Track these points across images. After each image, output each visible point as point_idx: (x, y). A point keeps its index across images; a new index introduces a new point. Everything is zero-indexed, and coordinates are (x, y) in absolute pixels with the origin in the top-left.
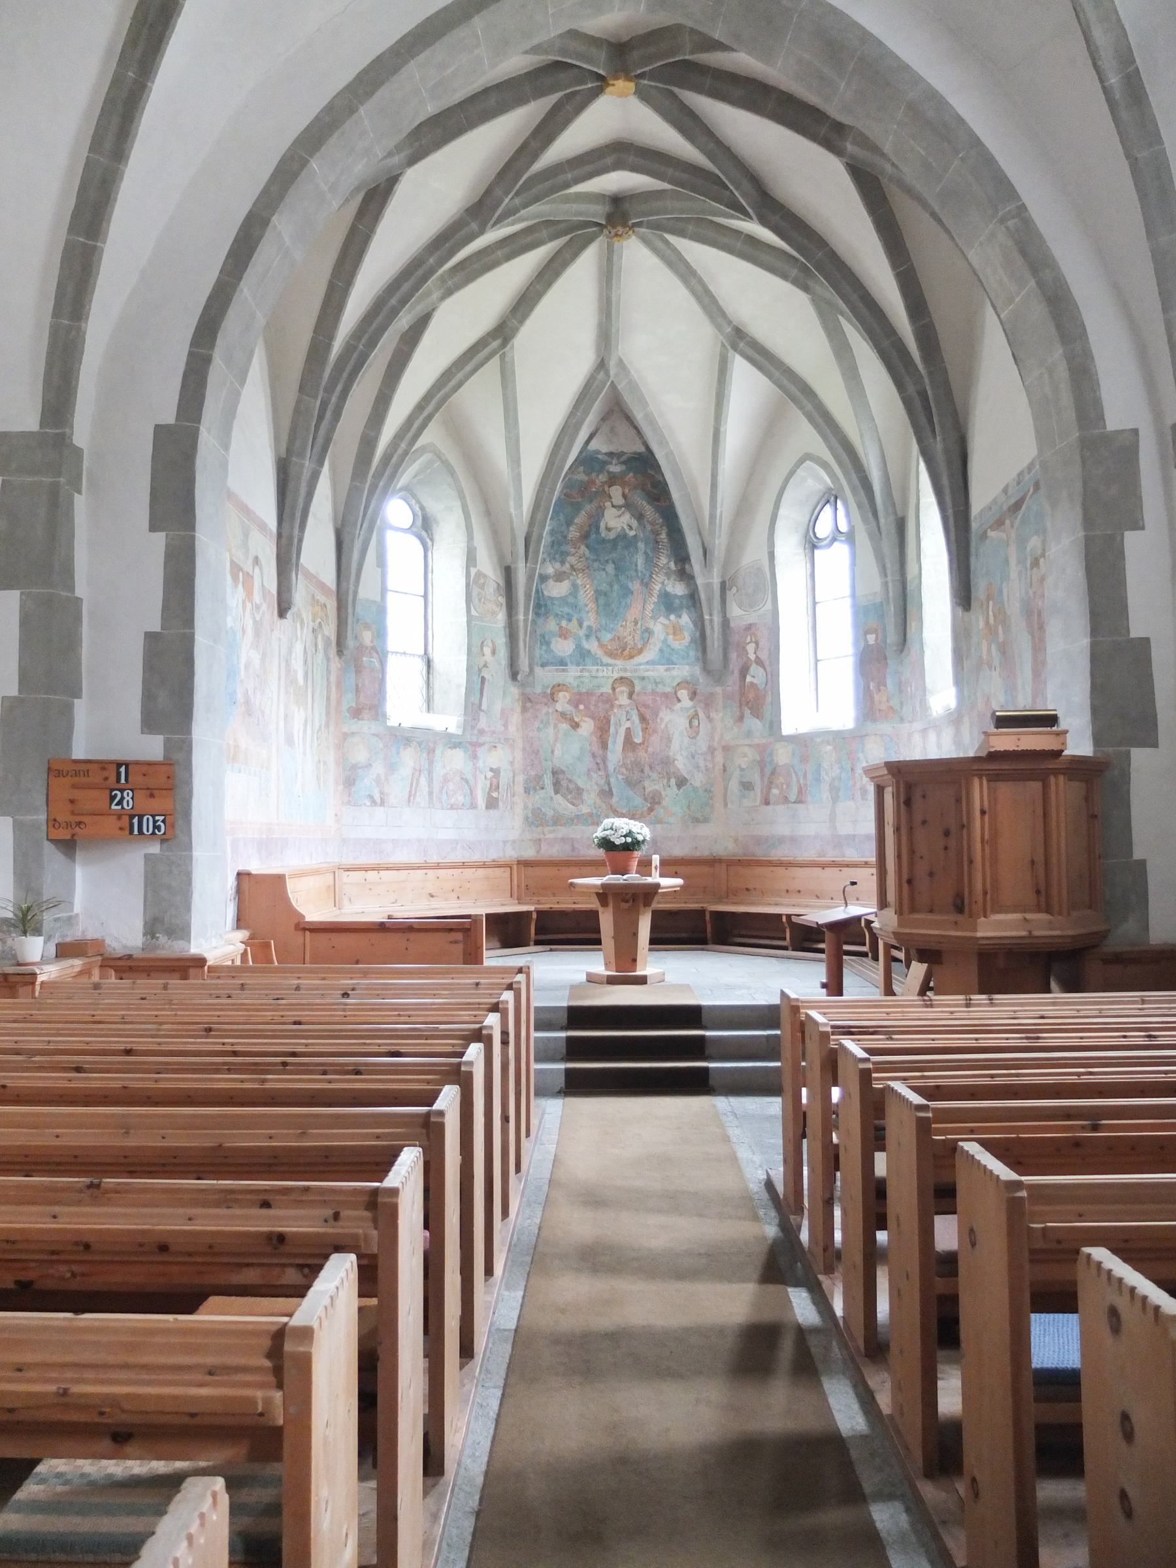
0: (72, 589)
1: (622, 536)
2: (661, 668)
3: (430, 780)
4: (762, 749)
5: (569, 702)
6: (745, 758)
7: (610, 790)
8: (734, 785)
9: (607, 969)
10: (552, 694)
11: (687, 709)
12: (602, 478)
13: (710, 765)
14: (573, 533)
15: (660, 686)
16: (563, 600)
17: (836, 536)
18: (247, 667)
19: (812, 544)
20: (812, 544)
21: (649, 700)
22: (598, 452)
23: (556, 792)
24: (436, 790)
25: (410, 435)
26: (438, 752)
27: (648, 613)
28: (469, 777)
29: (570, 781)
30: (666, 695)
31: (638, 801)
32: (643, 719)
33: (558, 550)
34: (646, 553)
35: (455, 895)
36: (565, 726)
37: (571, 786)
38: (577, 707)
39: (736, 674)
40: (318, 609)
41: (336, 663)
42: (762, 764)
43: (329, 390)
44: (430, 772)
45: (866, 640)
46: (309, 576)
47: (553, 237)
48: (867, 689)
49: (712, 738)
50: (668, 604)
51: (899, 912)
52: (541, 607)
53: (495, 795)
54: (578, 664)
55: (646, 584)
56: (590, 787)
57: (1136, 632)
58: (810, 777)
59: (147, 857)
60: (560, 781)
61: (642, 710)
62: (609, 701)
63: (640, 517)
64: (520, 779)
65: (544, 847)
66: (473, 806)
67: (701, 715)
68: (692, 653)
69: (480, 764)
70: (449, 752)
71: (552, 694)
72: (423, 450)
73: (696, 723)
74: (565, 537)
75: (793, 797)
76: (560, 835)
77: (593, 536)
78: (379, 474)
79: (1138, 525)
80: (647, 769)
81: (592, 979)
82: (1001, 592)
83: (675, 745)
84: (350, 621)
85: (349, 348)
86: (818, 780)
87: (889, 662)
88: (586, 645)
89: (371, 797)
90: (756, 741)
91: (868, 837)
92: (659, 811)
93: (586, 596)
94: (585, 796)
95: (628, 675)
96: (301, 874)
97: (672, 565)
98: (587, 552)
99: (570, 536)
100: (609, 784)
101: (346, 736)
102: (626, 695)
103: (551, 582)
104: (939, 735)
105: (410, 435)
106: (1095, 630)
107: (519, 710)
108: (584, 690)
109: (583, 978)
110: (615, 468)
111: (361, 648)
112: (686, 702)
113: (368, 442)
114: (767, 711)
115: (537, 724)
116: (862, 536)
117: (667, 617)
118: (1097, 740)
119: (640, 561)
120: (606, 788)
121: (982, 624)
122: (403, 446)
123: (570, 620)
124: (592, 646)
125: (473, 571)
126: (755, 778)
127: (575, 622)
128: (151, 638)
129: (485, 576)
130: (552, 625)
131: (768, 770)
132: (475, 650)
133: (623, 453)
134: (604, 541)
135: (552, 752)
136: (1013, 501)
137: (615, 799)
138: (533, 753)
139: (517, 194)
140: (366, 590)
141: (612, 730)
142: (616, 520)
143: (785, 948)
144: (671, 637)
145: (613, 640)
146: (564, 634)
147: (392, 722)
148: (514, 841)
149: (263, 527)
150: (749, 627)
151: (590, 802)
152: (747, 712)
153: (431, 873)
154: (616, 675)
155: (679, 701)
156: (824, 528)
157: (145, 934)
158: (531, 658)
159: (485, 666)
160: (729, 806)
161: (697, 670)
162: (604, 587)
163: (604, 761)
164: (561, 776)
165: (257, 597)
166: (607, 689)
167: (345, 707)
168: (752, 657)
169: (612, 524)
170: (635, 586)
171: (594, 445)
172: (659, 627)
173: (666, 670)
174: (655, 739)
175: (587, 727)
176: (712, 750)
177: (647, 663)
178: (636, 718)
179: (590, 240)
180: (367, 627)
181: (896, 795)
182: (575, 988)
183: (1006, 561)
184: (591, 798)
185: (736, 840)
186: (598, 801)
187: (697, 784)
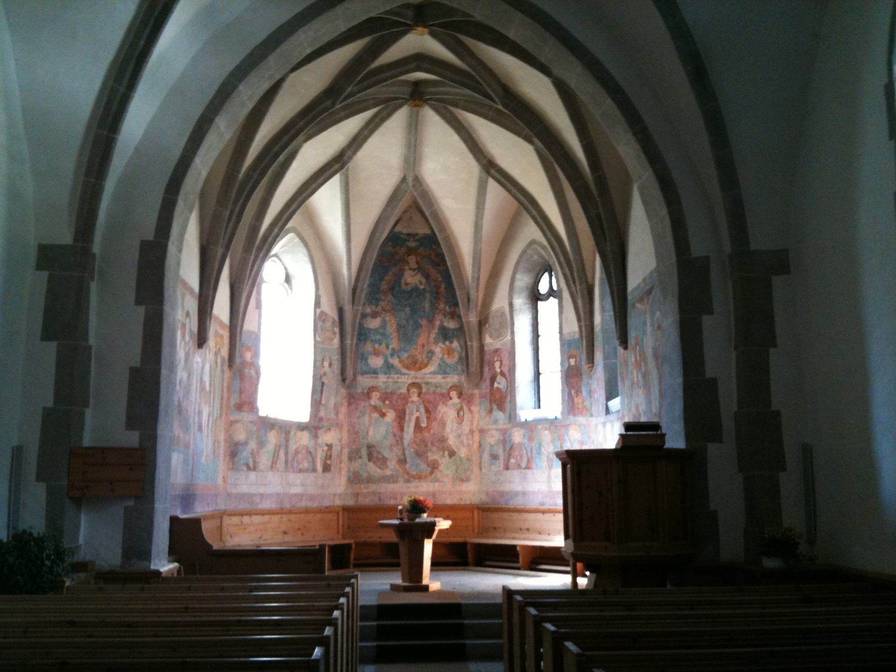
0: (87, 340)
1: (415, 289)
2: (440, 377)
3: (286, 453)
4: (504, 432)
5: (379, 399)
6: (493, 437)
7: (405, 458)
8: (486, 456)
9: (404, 581)
10: (368, 393)
11: (456, 404)
12: (403, 250)
13: (471, 442)
14: (384, 286)
15: (439, 389)
16: (376, 330)
17: (551, 293)
18: (180, 382)
19: (535, 297)
20: (535, 297)
21: (430, 397)
22: (401, 233)
23: (370, 460)
24: (290, 458)
25: (280, 224)
26: (292, 433)
27: (432, 340)
28: (312, 450)
29: (379, 453)
30: (442, 395)
31: (423, 466)
32: (427, 411)
33: (374, 296)
34: (431, 301)
35: (300, 533)
36: (376, 415)
37: (380, 456)
38: (384, 402)
39: (488, 382)
40: (219, 339)
41: (227, 374)
42: (504, 442)
43: (235, 203)
44: (287, 447)
45: (569, 363)
46: (217, 318)
47: (375, 106)
48: (570, 394)
49: (472, 424)
50: (445, 335)
51: (574, 541)
52: (362, 335)
53: (328, 462)
54: (385, 374)
55: (431, 321)
56: (392, 457)
57: (709, 374)
58: (534, 452)
59: (126, 508)
60: (373, 454)
61: (427, 404)
62: (405, 398)
63: (427, 276)
64: (346, 451)
65: (360, 499)
66: (314, 470)
67: (465, 408)
68: (459, 367)
69: (320, 441)
70: (299, 433)
71: (368, 393)
72: (288, 232)
73: (462, 413)
74: (378, 289)
75: (524, 465)
76: (371, 490)
77: (397, 289)
78: (260, 249)
79: (711, 312)
80: (429, 445)
81: (394, 588)
82: (642, 340)
83: (448, 428)
84: (238, 345)
85: (248, 176)
86: (539, 452)
87: (584, 377)
88: (391, 361)
89: (247, 465)
90: (501, 427)
91: (558, 492)
92: (438, 474)
93: (391, 328)
94: (389, 463)
95: (418, 381)
96: (206, 517)
97: (447, 308)
98: (393, 299)
99: (382, 288)
100: (404, 454)
101: (232, 423)
102: (416, 395)
103: (369, 319)
104: (612, 426)
105: (280, 224)
106: (686, 373)
107: (346, 404)
108: (389, 391)
109: (388, 587)
110: (412, 244)
111: (244, 364)
112: (456, 400)
113: (255, 229)
114: (508, 406)
115: (358, 414)
116: (566, 295)
117: (444, 343)
118: (688, 437)
119: (427, 305)
120: (402, 457)
121: (633, 359)
122: (276, 230)
123: (380, 344)
124: (395, 361)
125: (318, 311)
126: (500, 452)
127: (384, 345)
128: (134, 371)
129: (326, 315)
130: (369, 347)
131: (508, 447)
132: (318, 364)
133: (417, 234)
134: (404, 292)
135: (368, 433)
136: (648, 287)
137: (408, 466)
138: (354, 433)
139: (356, 85)
140: (249, 324)
141: (407, 418)
142: (411, 278)
143: (519, 569)
144: (446, 356)
145: (408, 357)
146: (376, 353)
147: (262, 413)
148: (340, 495)
149: (191, 291)
150: (496, 351)
151: (392, 467)
152: (495, 407)
153: (285, 518)
154: (410, 381)
155: (451, 399)
156: (543, 288)
157: (123, 557)
158: (355, 369)
159: (325, 374)
160: (483, 470)
161: (463, 378)
162: (403, 322)
163: (402, 438)
164: (372, 449)
165: (187, 338)
166: (404, 390)
167: (232, 402)
168: (498, 370)
169: (409, 280)
170: (424, 322)
171: (398, 229)
172: (438, 350)
173: (444, 378)
174: (435, 424)
175: (391, 416)
176: (472, 432)
177: (430, 373)
178: (422, 409)
179: (399, 107)
180: (248, 349)
181: (572, 469)
182: (382, 593)
183: (645, 323)
184: (392, 464)
185: (487, 494)
186: (397, 467)
187: (463, 455)
